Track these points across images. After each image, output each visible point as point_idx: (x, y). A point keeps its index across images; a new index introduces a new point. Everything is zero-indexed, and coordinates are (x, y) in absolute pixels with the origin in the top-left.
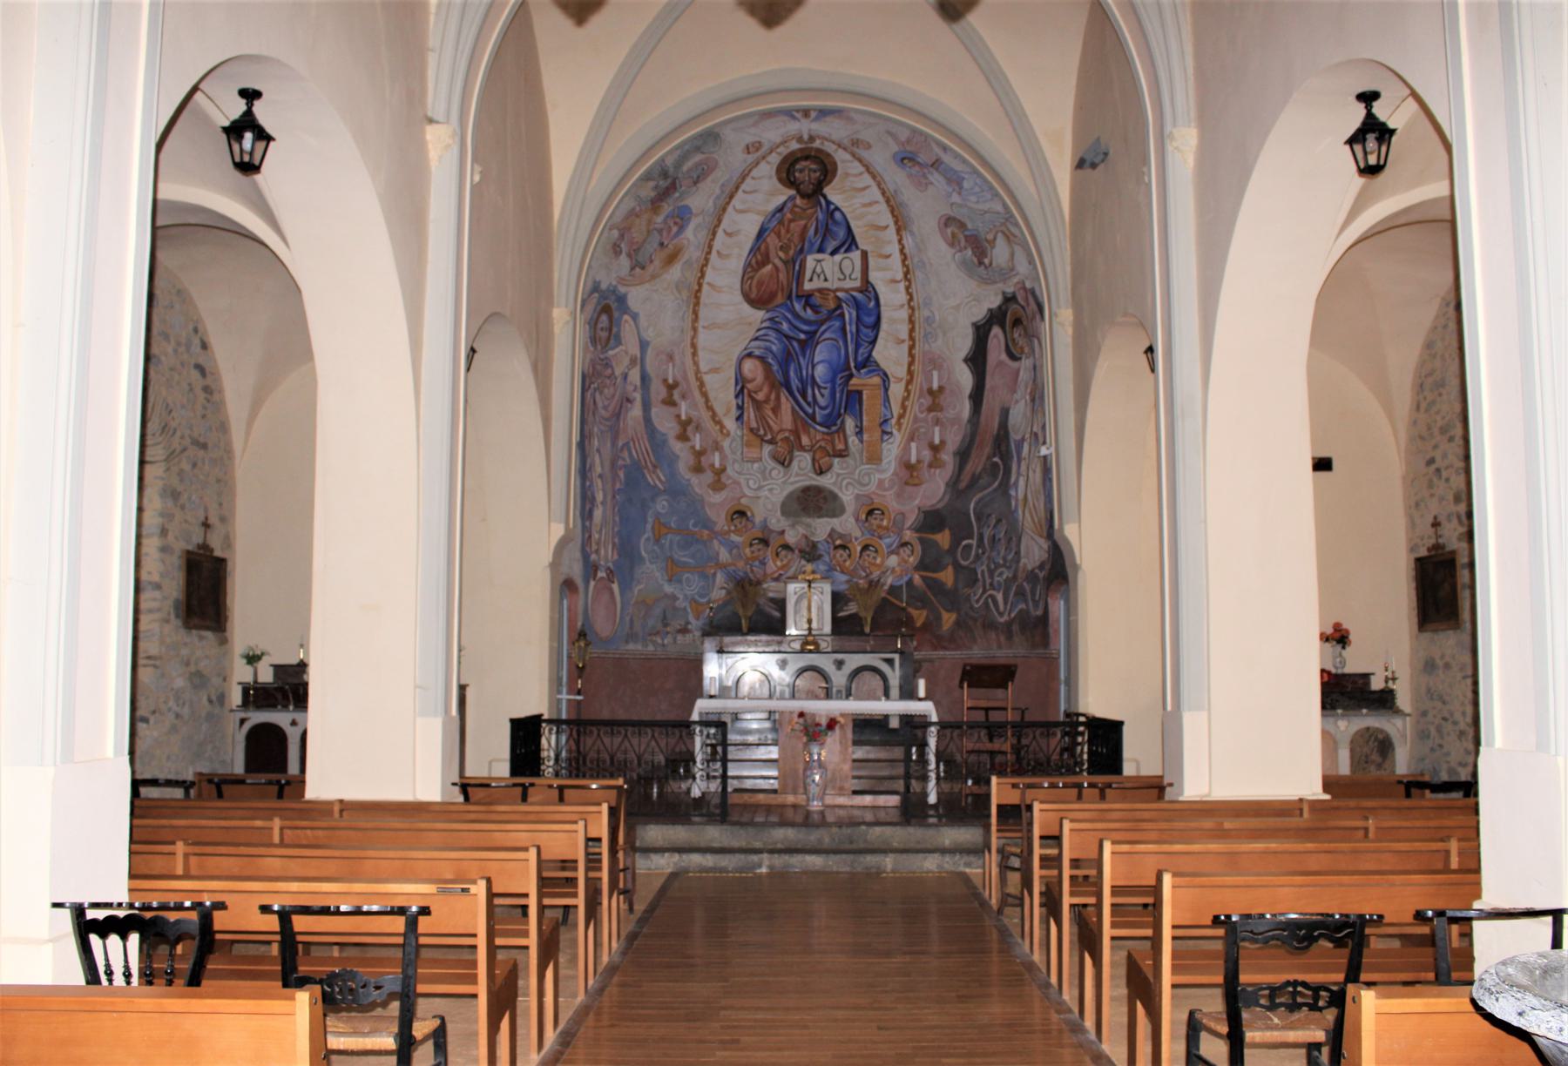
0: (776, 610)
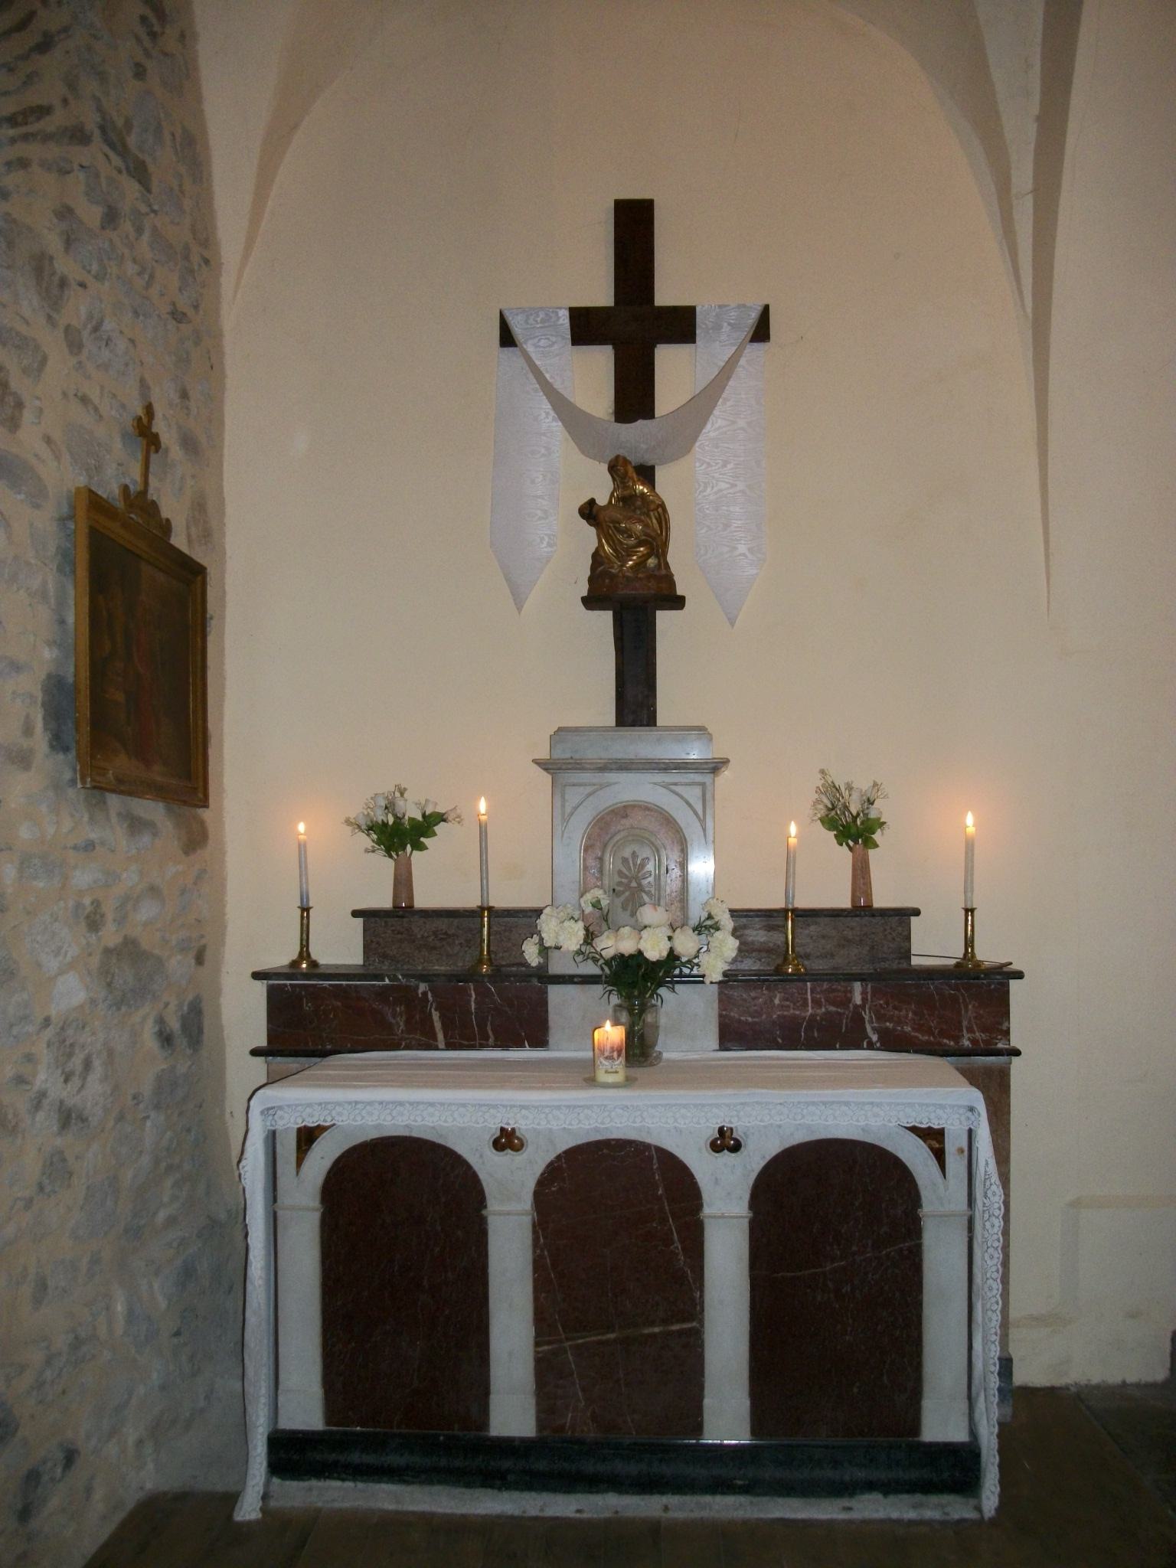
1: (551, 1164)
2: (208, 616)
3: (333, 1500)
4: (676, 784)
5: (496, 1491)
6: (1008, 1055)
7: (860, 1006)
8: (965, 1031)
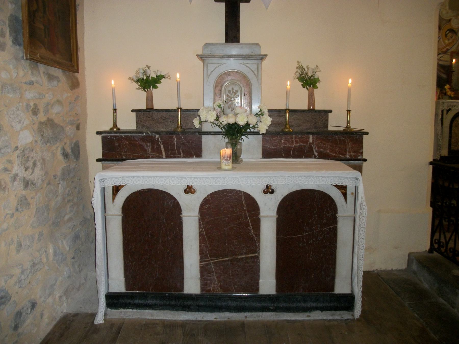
0: (444, 73)
1: (205, 198)
2: (77, 4)
3: (129, 316)
4: (248, 64)
5: (186, 312)
6: (362, 161)
7: (312, 143)
8: (347, 152)
